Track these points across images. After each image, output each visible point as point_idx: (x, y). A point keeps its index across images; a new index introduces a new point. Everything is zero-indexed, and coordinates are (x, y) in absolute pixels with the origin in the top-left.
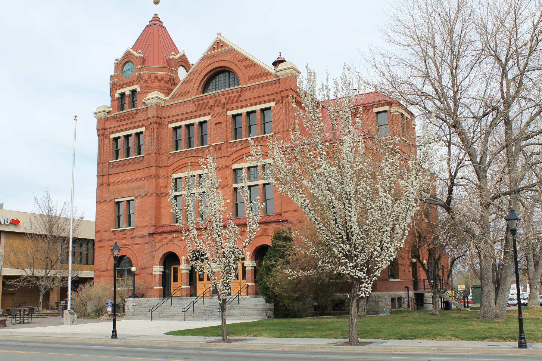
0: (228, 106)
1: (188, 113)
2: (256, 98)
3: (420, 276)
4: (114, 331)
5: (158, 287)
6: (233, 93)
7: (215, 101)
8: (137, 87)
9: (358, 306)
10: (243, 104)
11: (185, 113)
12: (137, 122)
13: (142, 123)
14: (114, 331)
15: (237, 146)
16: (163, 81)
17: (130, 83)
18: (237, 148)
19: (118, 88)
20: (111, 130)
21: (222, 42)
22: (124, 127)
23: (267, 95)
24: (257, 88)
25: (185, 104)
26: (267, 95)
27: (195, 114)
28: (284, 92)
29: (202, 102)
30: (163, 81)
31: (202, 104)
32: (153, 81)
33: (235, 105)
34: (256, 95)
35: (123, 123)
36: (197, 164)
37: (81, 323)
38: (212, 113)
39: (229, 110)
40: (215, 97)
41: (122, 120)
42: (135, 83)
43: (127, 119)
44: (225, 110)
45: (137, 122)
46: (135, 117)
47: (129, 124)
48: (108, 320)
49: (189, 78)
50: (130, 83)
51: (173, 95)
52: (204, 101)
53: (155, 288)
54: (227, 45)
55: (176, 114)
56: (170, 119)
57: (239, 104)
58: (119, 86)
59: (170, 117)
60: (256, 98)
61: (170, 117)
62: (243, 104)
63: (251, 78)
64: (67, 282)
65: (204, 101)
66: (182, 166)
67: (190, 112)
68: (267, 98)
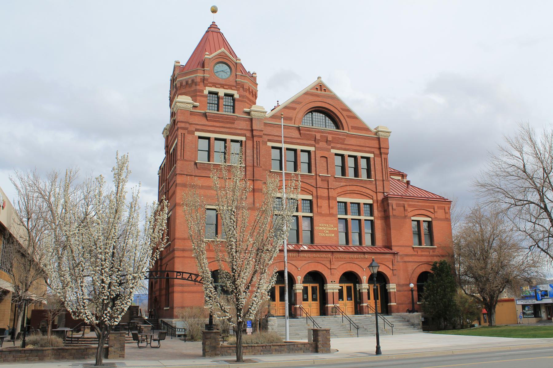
0: (332, 145)
1: (291, 138)
2: (358, 146)
4: (378, 348)
5: (392, 304)
6: (340, 135)
10: (347, 147)
11: (288, 137)
13: (243, 132)
14: (378, 348)
15: (341, 182)
17: (226, 85)
19: (209, 85)
20: (198, 127)
21: (325, 86)
22: (217, 129)
23: (368, 147)
24: (354, 137)
25: (288, 128)
26: (368, 147)
27: (298, 141)
28: (181, 124)
29: (308, 133)
31: (308, 134)
33: (339, 146)
34: (358, 143)
37: (411, 333)
39: (333, 148)
43: (222, 122)
44: (330, 147)
47: (224, 127)
48: (234, 355)
49: (291, 106)
50: (226, 85)
52: (311, 133)
53: (395, 304)
54: (330, 91)
56: (270, 138)
57: (343, 146)
58: (211, 83)
59: (270, 135)
60: (358, 146)
61: (270, 135)
62: (347, 147)
63: (354, 128)
65: (311, 133)
66: (347, 192)
67: (293, 138)
68: (367, 149)
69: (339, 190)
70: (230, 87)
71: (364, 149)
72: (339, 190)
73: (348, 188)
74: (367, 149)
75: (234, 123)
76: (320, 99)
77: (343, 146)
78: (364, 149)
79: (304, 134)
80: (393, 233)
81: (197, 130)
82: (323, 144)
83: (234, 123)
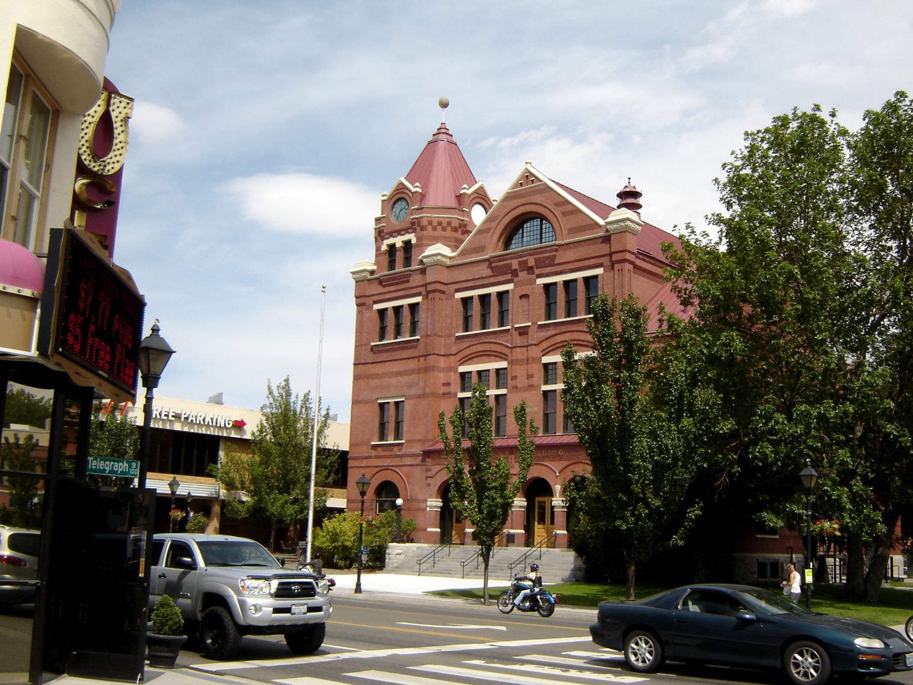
1: (483, 278)
7: (520, 263)
8: (412, 237)
10: (559, 268)
14: (358, 584)
20: (376, 298)
27: (492, 280)
30: (449, 228)
32: (434, 229)
33: (548, 270)
34: (576, 257)
35: (392, 288)
39: (539, 276)
47: (398, 290)
50: (402, 230)
54: (13, 66)
57: (553, 269)
58: (387, 234)
62: (559, 268)
63: (574, 231)
68: (592, 262)
69: (545, 345)
70: (406, 231)
71: (587, 263)
72: (545, 345)
73: (559, 339)
74: (592, 262)
75: (408, 281)
76: (523, 201)
77: (553, 269)
78: (587, 263)
79: (497, 267)
80: (151, 364)
81: (375, 302)
82: (523, 275)
83: (408, 281)
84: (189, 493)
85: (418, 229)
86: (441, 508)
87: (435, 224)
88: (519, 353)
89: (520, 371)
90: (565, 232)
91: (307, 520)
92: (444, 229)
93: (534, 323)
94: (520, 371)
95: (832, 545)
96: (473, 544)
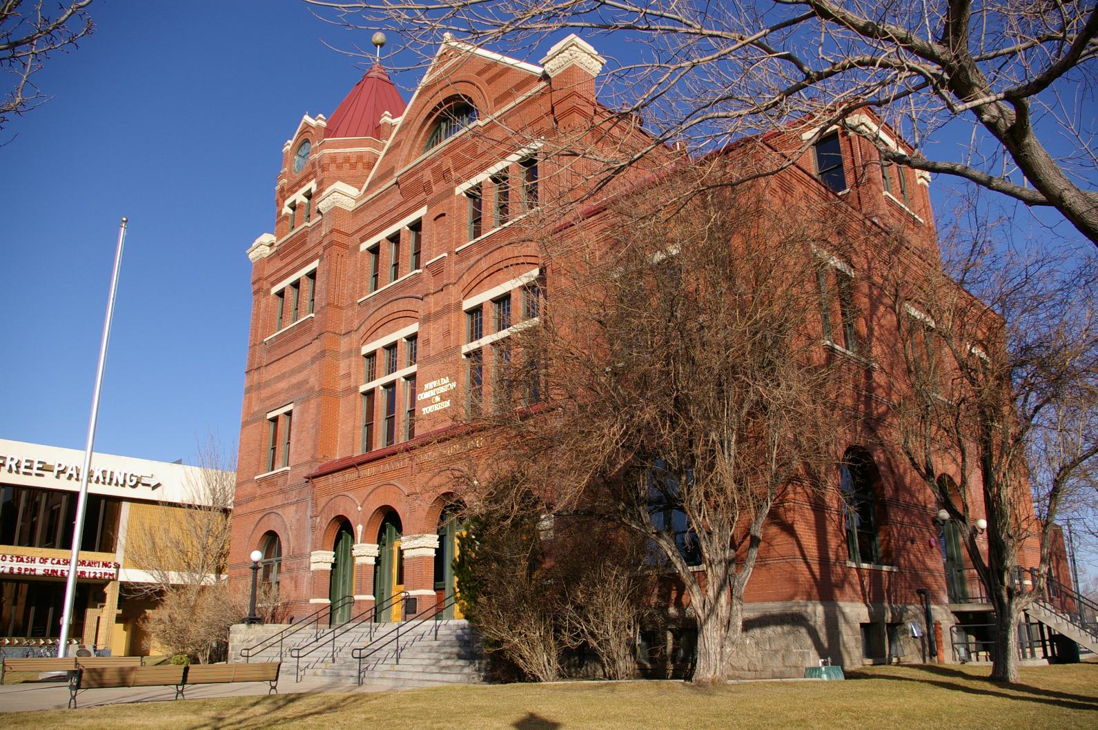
1: (391, 211)
3: (813, 151)
7: (434, 171)
8: (312, 185)
9: (926, 681)
12: (308, 251)
16: (360, 165)
18: (472, 260)
20: (273, 278)
27: (401, 210)
30: (360, 165)
32: (339, 167)
35: (288, 259)
36: (413, 314)
38: (429, 198)
40: (433, 161)
41: (288, 255)
42: (302, 183)
43: (295, 250)
45: (308, 251)
46: (304, 243)
47: (296, 259)
50: (300, 181)
51: (370, 183)
53: (312, 601)
55: (371, 219)
64: (33, 630)
66: (378, 325)
69: (466, 279)
84: (793, 524)
85: (319, 171)
86: (436, 550)
87: (340, 160)
88: (432, 304)
89: (433, 332)
90: (490, 104)
91: (34, 625)
92: (353, 166)
93: (450, 253)
94: (433, 332)
95: (33, 609)
96: (782, 536)
